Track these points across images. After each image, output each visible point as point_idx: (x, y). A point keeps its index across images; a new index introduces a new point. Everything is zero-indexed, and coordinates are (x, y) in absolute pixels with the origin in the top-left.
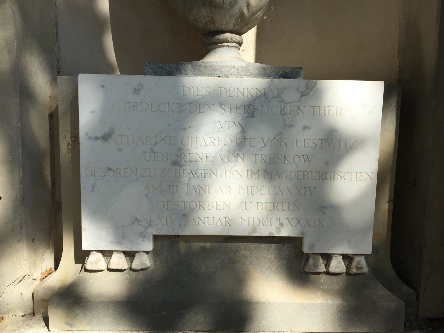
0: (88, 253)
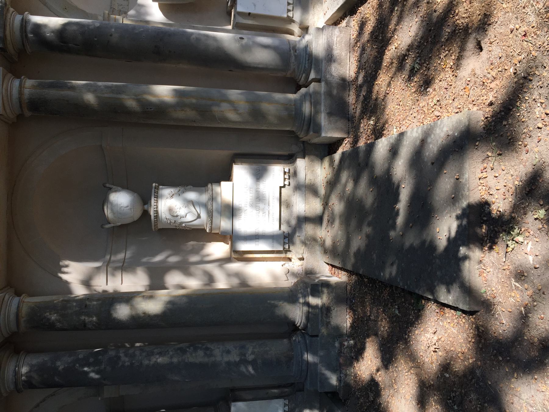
0: (288, 16)
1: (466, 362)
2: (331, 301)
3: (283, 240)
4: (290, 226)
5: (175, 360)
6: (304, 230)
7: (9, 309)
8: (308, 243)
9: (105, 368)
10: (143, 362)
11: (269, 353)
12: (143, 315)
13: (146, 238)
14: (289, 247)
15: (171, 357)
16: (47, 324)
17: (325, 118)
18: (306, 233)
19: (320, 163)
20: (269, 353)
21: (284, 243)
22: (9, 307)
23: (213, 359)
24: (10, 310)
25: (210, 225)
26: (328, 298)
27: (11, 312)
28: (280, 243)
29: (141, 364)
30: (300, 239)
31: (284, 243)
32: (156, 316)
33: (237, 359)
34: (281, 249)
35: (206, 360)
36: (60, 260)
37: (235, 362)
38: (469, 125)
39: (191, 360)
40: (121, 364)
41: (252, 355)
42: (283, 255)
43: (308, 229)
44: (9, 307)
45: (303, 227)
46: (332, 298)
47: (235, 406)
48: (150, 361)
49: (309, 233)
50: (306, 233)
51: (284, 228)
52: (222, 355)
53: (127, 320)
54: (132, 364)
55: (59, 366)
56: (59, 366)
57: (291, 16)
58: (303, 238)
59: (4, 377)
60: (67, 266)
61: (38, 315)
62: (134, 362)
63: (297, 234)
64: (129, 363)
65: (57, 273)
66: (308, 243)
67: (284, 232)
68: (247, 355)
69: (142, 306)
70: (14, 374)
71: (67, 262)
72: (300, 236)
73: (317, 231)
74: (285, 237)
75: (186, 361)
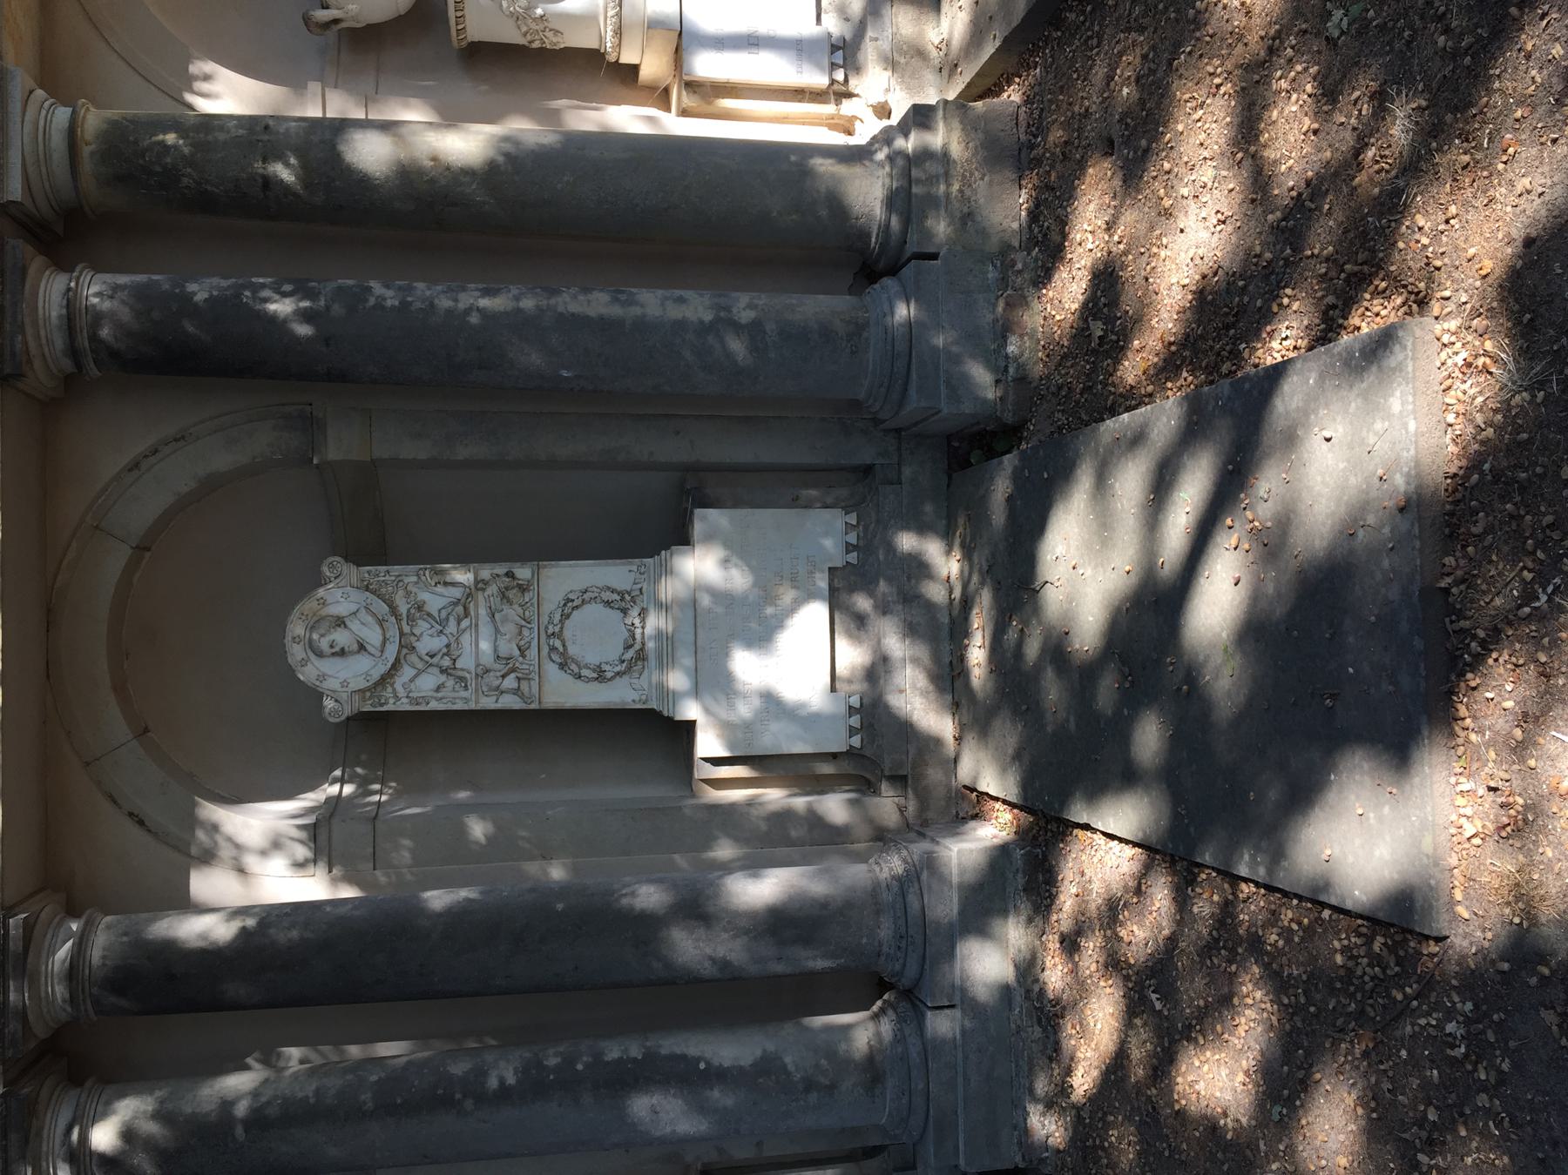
1: (1435, 1072)
2: (973, 155)
3: (830, 58)
4: (847, 20)
5: (528, 303)
6: (889, 25)
7: (46, 117)
8: (903, 61)
9: (328, 308)
10: (436, 301)
11: (798, 309)
12: (432, 163)
13: (431, 83)
14: (846, 80)
15: (517, 298)
16: (158, 169)
17: (966, 841)
18: (895, 30)
19: (932, 15)
20: (798, 309)
21: (833, 66)
22: (48, 113)
23: (636, 311)
24: (51, 121)
25: (614, 8)
26: (963, 144)
27: (53, 126)
28: (818, 66)
29: (432, 305)
30: (876, 48)
31: (833, 66)
32: (467, 172)
33: (708, 317)
34: (819, 80)
35: (616, 311)
36: (188, 60)
37: (701, 322)
38: (1418, 475)
39: (574, 308)
40: (372, 301)
41: (748, 311)
42: (828, 109)
43: (900, 20)
44: (48, 113)
45: (884, 12)
46: (976, 147)
47: (704, 519)
48: (456, 300)
49: (903, 32)
50: (895, 30)
51: (832, 25)
52: (662, 304)
53: (387, 177)
54: (405, 305)
55: (194, 294)
56: (194, 294)
57: (842, 644)
58: (885, 45)
59: (37, 307)
60: (207, 78)
61: (131, 138)
62: (409, 299)
63: (870, 33)
64: (397, 303)
65: (180, 91)
66: (903, 61)
67: (830, 35)
68: (735, 310)
69: (429, 139)
70: (65, 302)
71: (209, 67)
72: (876, 39)
73: (925, 27)
74: (834, 48)
75: (561, 309)
